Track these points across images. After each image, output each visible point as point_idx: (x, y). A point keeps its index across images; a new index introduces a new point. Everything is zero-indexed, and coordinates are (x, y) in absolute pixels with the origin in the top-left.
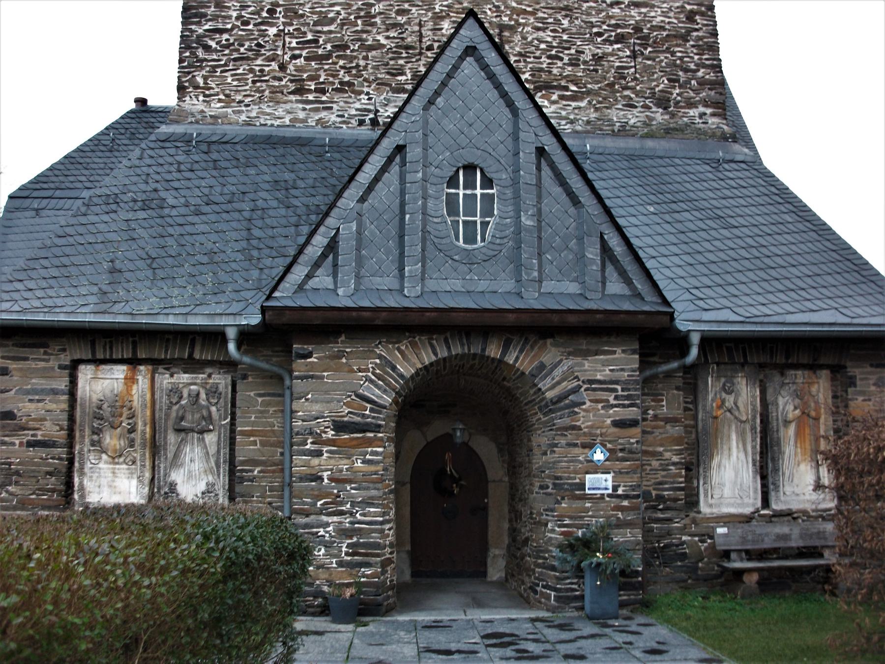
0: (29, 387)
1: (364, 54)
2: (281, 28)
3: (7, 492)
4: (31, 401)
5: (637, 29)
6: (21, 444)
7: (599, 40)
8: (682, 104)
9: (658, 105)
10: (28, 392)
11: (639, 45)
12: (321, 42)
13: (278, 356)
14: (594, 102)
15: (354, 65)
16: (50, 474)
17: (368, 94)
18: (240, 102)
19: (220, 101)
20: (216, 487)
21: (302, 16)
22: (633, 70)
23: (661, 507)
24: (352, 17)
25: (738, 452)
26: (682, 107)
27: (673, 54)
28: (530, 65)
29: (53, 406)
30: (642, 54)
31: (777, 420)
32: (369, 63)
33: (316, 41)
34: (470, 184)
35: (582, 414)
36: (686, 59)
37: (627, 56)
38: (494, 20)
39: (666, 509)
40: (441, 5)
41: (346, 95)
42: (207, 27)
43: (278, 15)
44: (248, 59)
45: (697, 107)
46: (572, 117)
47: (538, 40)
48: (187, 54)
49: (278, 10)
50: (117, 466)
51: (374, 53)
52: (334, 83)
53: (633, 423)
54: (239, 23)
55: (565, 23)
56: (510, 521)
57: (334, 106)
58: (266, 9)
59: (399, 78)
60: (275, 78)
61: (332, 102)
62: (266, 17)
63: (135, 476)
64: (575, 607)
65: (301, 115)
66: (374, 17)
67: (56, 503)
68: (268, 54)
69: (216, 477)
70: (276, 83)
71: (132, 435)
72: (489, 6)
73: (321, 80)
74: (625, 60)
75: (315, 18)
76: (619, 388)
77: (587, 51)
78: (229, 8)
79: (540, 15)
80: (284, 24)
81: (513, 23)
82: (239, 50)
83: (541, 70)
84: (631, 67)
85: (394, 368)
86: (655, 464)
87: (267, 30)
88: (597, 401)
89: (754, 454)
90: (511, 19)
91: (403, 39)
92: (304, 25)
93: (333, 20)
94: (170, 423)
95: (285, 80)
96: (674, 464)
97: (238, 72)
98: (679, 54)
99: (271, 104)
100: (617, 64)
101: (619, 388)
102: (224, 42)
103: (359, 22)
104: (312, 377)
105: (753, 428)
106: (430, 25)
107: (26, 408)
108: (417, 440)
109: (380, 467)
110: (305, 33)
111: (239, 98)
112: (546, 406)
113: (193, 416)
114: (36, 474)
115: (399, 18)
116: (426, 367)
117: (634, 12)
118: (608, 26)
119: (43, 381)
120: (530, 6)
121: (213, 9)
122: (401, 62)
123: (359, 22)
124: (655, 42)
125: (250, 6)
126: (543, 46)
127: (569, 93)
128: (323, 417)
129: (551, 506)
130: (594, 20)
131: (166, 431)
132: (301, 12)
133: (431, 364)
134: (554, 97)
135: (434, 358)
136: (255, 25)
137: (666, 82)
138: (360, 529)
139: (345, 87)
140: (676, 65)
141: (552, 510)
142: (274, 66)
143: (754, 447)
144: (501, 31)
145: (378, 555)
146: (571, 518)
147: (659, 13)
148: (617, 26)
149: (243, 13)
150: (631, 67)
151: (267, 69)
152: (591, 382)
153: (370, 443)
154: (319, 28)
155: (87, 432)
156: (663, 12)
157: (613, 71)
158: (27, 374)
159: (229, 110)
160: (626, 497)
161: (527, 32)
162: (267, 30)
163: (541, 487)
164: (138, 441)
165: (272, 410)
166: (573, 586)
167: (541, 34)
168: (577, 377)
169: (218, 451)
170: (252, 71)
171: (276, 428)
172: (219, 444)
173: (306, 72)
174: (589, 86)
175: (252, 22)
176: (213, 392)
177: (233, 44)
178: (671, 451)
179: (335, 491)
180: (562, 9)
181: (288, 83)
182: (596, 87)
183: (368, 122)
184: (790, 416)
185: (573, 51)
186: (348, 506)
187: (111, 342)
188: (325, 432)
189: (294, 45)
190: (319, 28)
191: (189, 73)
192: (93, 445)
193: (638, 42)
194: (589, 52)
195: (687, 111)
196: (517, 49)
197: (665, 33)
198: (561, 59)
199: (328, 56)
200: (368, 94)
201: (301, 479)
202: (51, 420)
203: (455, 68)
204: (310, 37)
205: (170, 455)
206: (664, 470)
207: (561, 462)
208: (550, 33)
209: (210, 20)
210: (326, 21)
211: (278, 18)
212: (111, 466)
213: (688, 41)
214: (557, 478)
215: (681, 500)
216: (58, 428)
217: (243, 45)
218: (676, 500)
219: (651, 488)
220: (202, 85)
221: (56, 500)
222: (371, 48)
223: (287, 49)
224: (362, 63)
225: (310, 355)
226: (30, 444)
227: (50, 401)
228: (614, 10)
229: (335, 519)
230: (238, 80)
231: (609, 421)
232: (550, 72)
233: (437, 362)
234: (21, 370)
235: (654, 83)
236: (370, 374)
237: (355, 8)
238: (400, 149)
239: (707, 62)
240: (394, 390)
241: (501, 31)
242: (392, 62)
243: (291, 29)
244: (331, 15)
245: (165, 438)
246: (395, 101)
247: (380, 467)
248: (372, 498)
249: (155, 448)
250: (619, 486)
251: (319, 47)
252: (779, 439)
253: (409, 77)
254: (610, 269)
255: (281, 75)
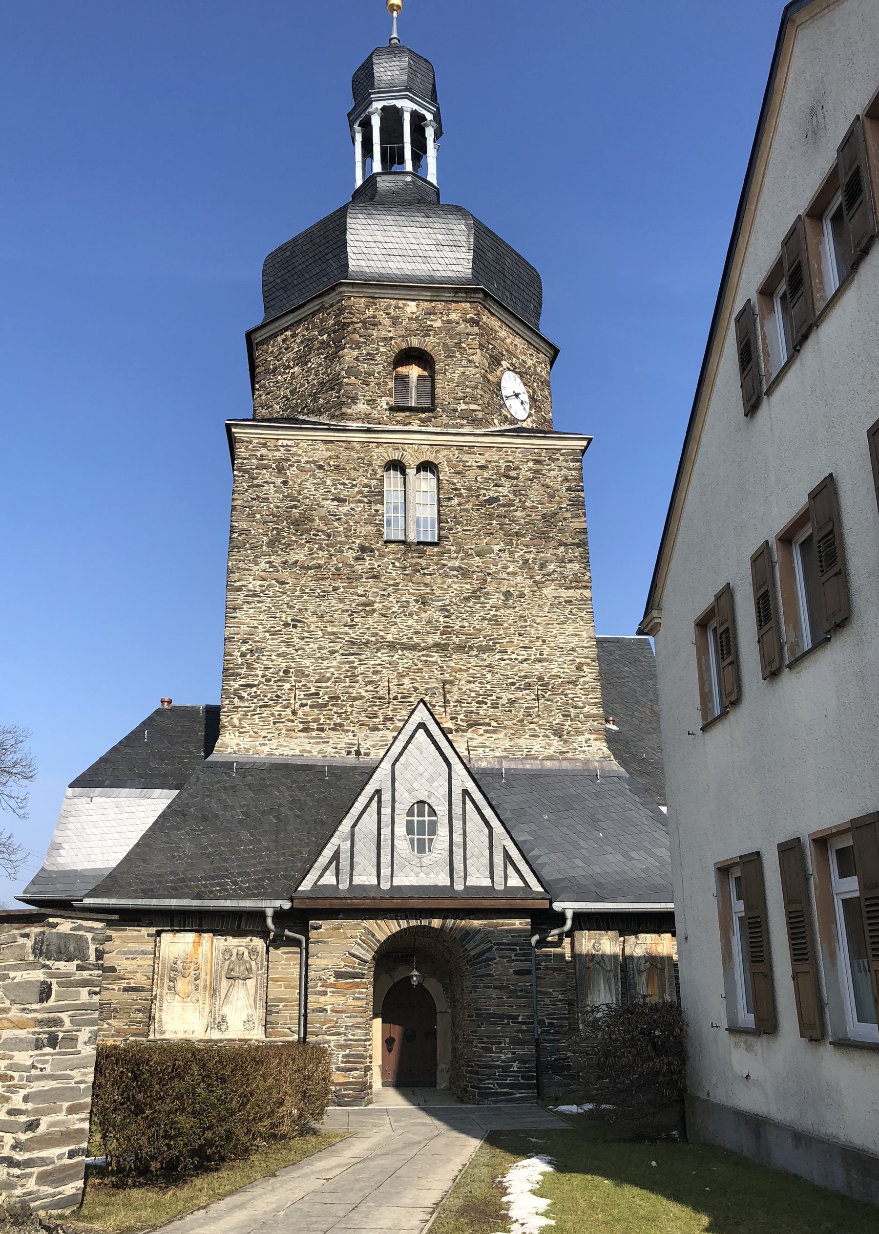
0: (126, 949)
1: (351, 703)
2: (294, 684)
3: (107, 1024)
4: (127, 959)
5: (540, 679)
6: (119, 990)
7: (513, 688)
8: (572, 733)
9: (555, 735)
10: (125, 953)
11: (542, 690)
12: (321, 695)
13: (296, 926)
14: (509, 734)
15: (343, 711)
16: (139, 1010)
17: (353, 732)
18: (264, 737)
19: (250, 736)
20: (254, 1018)
21: (308, 675)
22: (537, 709)
23: (552, 1031)
24: (342, 676)
25: (605, 992)
26: (572, 735)
27: (566, 695)
28: (464, 709)
29: (143, 963)
30: (544, 697)
31: (633, 970)
32: (355, 710)
33: (317, 694)
34: (421, 814)
35: (494, 966)
36: (575, 699)
37: (533, 699)
38: (440, 676)
39: (557, 1033)
40: (403, 667)
41: (339, 733)
42: (240, 683)
43: (291, 675)
44: (270, 706)
45: (584, 735)
46: (493, 746)
47: (469, 690)
48: (227, 702)
49: (291, 670)
50: (186, 1004)
51: (357, 702)
52: (330, 724)
53: (528, 972)
54: (263, 680)
55: (489, 676)
56: (452, 1042)
57: (330, 740)
58: (282, 670)
59: (374, 720)
60: (289, 720)
61: (329, 738)
62: (283, 676)
63: (198, 1011)
64: (491, 1101)
65: (308, 747)
66: (357, 676)
67: (142, 1031)
68: (284, 703)
69: (254, 1010)
70: (290, 724)
71: (197, 982)
72: (436, 667)
73: (321, 722)
74: (531, 702)
75: (317, 677)
76: (518, 948)
77: (504, 697)
78: (256, 669)
79: (471, 671)
80: (296, 681)
81: (452, 678)
82: (263, 700)
83: (471, 712)
84: (536, 707)
85: (373, 936)
86: (547, 1001)
87: (283, 686)
88: (503, 957)
89: (617, 994)
90: (451, 676)
91: (377, 692)
92: (309, 682)
93: (329, 679)
94: (224, 973)
95: (296, 722)
96: (560, 1001)
97: (263, 715)
98: (570, 695)
99: (286, 739)
100: (526, 705)
101: (518, 948)
102: (253, 694)
103: (347, 680)
104: (321, 942)
105: (616, 976)
106: (395, 682)
107: (123, 964)
108: (388, 983)
109: (364, 1003)
110: (310, 688)
111: (264, 734)
112: (471, 960)
113: (239, 967)
114: (129, 1011)
115: (374, 677)
116: (393, 935)
117: (538, 666)
118: (519, 677)
119: (136, 945)
120: (464, 665)
121: (245, 670)
122: (376, 708)
123: (347, 680)
124: (553, 688)
125: (271, 668)
126: (473, 694)
127: (491, 728)
128: (328, 969)
129: (475, 1029)
130: (509, 673)
131: (221, 979)
132: (307, 672)
133: (397, 933)
134: (481, 732)
135: (399, 929)
136: (275, 682)
137: (561, 717)
138: (351, 1045)
139: (337, 727)
140: (568, 704)
141: (475, 1032)
142: (289, 711)
143: (617, 990)
144: (444, 685)
145: (362, 1063)
146: (488, 1037)
147: (556, 665)
148: (526, 677)
149: (266, 673)
150: (536, 707)
151: (283, 713)
152: (499, 944)
153: (358, 986)
154: (319, 684)
155: (166, 980)
156: (559, 665)
157: (523, 710)
158: (124, 940)
159: (257, 743)
160: (525, 1023)
161: (462, 685)
162: (283, 686)
163: (469, 1016)
164: (201, 986)
165: (292, 963)
166: (490, 1086)
167: (472, 685)
168: (490, 941)
169: (256, 993)
170: (273, 715)
171: (295, 976)
172: (256, 987)
173: (310, 716)
174: (505, 723)
175: (273, 679)
176: (253, 952)
177: (259, 696)
178: (557, 991)
179: (335, 1019)
180: (487, 666)
181: (298, 724)
182: (510, 723)
183: (354, 753)
184: (642, 968)
185: (494, 697)
186: (343, 1029)
187: (184, 918)
188: (329, 979)
189: (302, 696)
190: (319, 684)
191: (228, 716)
192: (169, 989)
193: (541, 688)
194: (506, 696)
195: (577, 737)
196: (456, 697)
197: (561, 680)
198: (486, 703)
199: (326, 705)
200: (353, 732)
201: (313, 1011)
202: (141, 972)
203: (412, 737)
204: (313, 690)
205: (223, 996)
206: (553, 1005)
207: (481, 998)
208: (478, 685)
209: (243, 678)
210: (324, 679)
211: (291, 677)
212: (182, 1004)
213: (578, 685)
214: (478, 1010)
215: (566, 1026)
216: (146, 978)
217: (266, 696)
218: (562, 1026)
219: (545, 1018)
220: (237, 725)
221: (142, 1029)
222: (355, 699)
223: (297, 700)
224: (349, 709)
225: (320, 927)
226: (126, 990)
227: (140, 959)
228: (523, 665)
229: (335, 1038)
230: (263, 721)
231: (511, 971)
232: (478, 713)
233: (401, 931)
234: (120, 937)
235: (552, 718)
236: (358, 940)
237: (343, 670)
238: (378, 792)
239: (591, 701)
240: (373, 950)
241: (444, 685)
242: (370, 709)
243: (300, 684)
244: (328, 675)
245: (220, 983)
246: (372, 737)
247: (364, 1003)
248: (359, 1023)
249: (214, 992)
250: (519, 1015)
251: (320, 698)
252: (635, 984)
253: (382, 720)
254: (510, 869)
255: (293, 718)
